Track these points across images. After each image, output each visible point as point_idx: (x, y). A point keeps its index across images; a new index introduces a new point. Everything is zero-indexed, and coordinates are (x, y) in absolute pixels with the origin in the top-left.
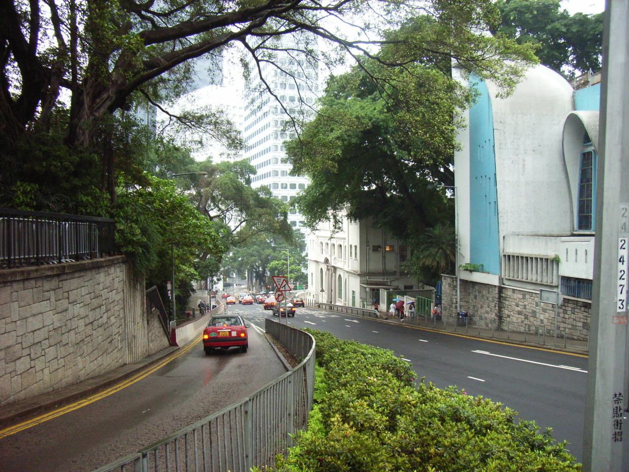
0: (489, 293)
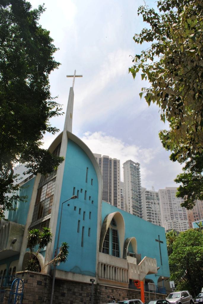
0: (82, 290)
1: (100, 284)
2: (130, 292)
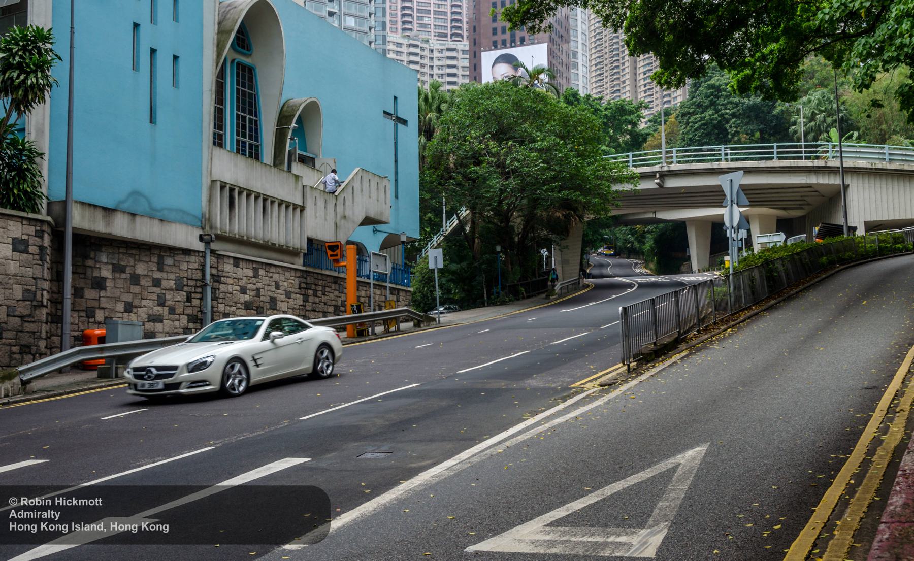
0: (160, 269)
1: (218, 253)
2: (308, 278)
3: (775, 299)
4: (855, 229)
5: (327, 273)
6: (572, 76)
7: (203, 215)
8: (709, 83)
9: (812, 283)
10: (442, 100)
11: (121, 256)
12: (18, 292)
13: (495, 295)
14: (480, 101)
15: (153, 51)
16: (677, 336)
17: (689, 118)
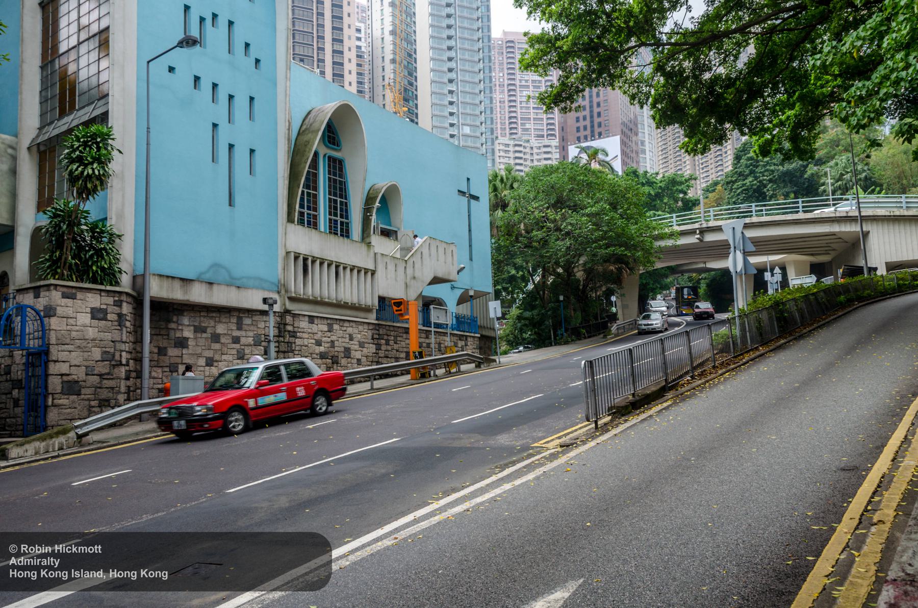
2: (381, 330)
3: (786, 338)
4: (875, 269)
5: (398, 325)
6: (641, 160)
7: (279, 281)
8: (748, 155)
9: (827, 320)
10: (515, 180)
11: (202, 319)
12: (97, 354)
13: (560, 336)
14: (541, 178)
15: (231, 146)
16: (664, 384)
17: (732, 185)
